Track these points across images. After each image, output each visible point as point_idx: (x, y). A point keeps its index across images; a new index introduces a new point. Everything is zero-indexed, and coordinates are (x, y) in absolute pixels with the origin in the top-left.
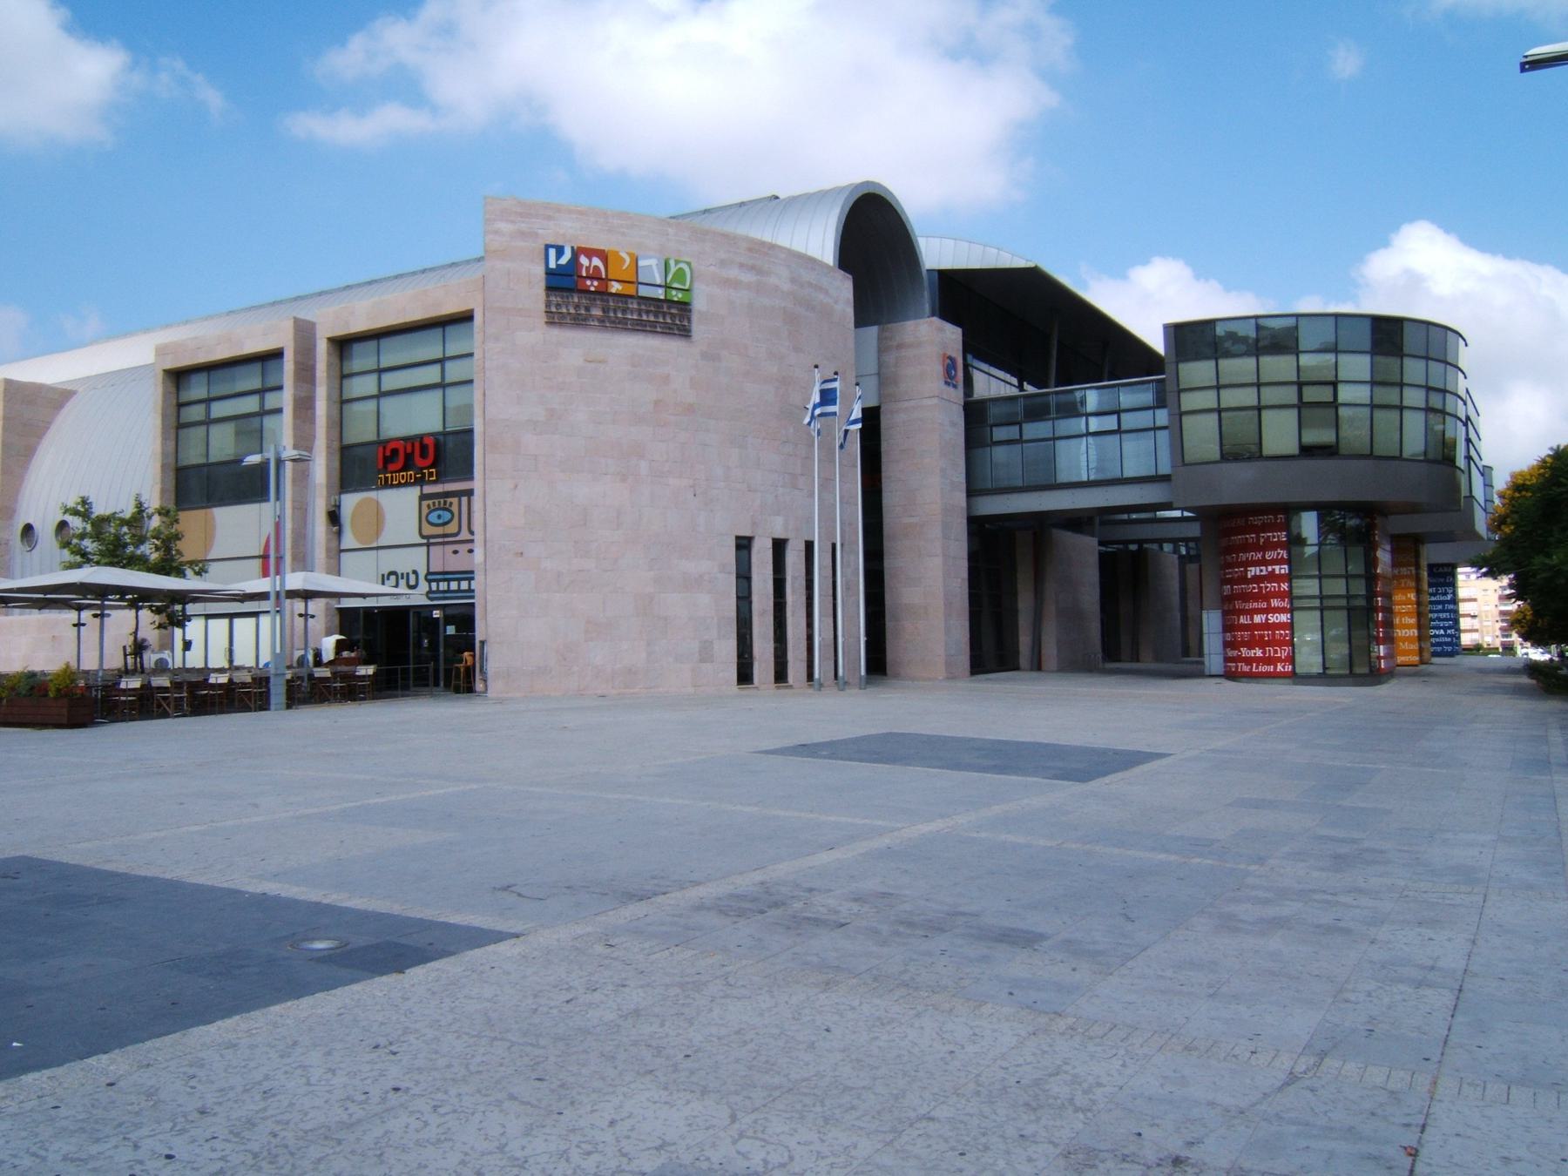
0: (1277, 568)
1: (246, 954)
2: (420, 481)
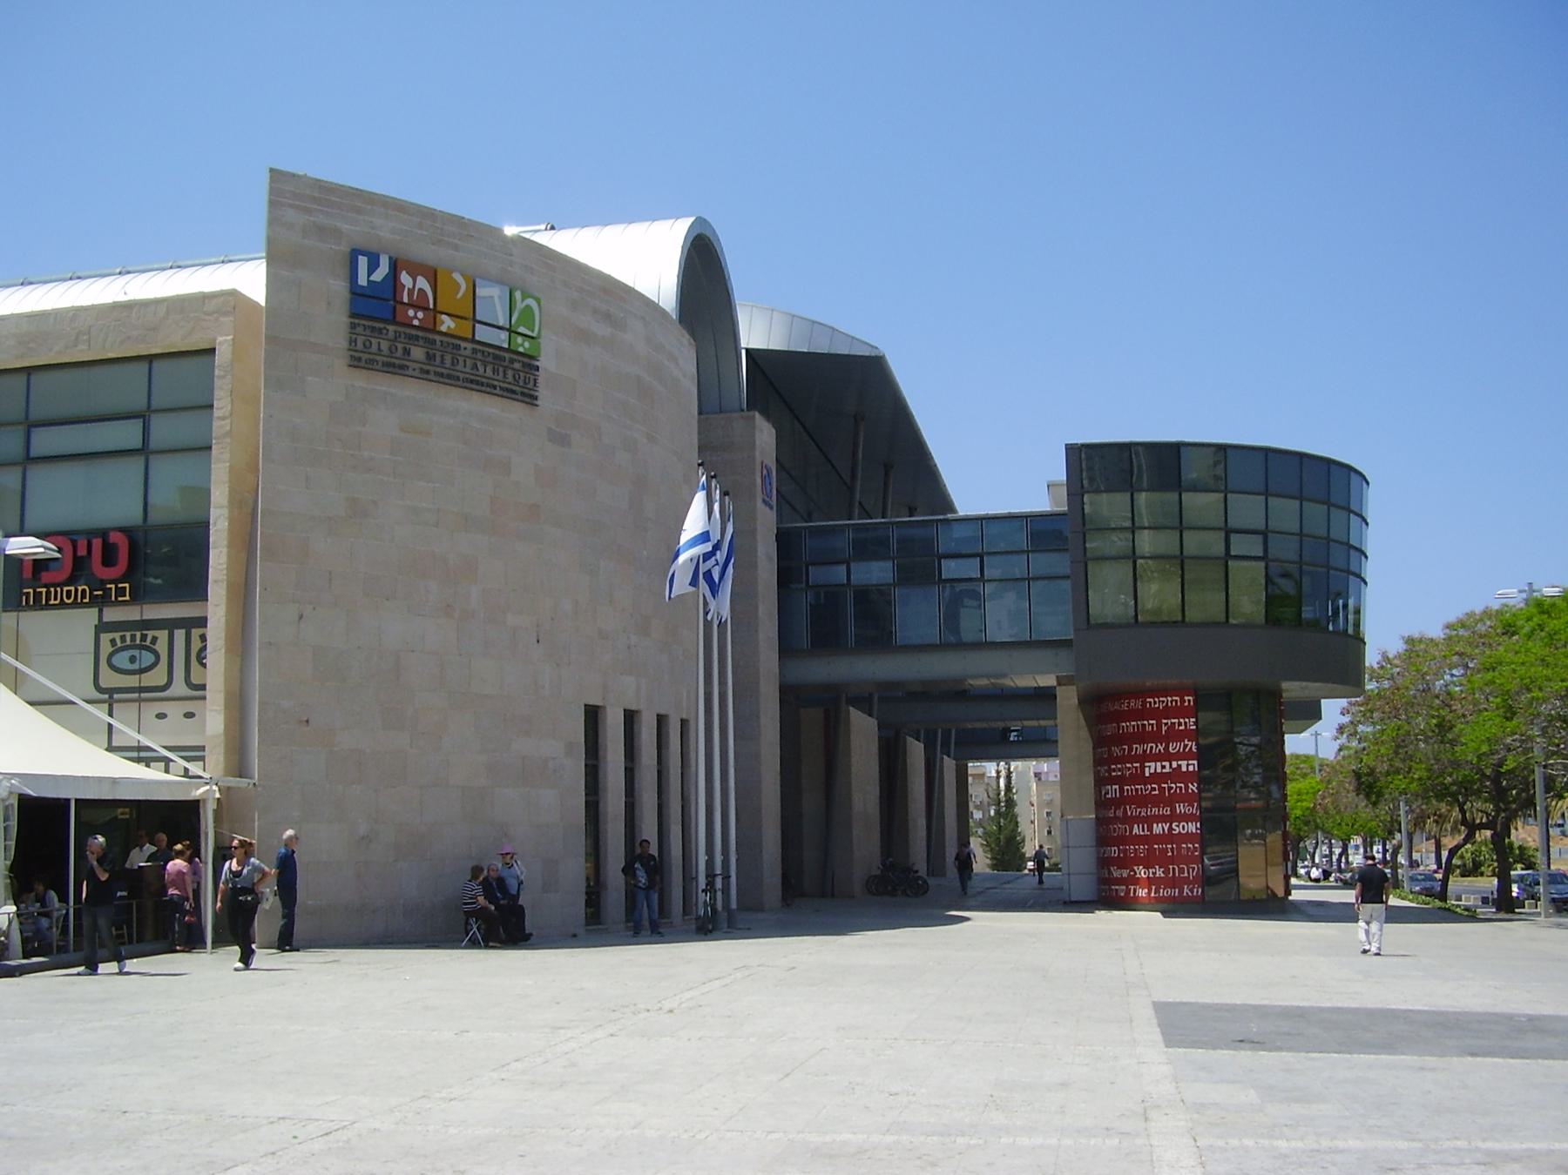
0: (1183, 763)
1: (967, 919)
2: (100, 602)
